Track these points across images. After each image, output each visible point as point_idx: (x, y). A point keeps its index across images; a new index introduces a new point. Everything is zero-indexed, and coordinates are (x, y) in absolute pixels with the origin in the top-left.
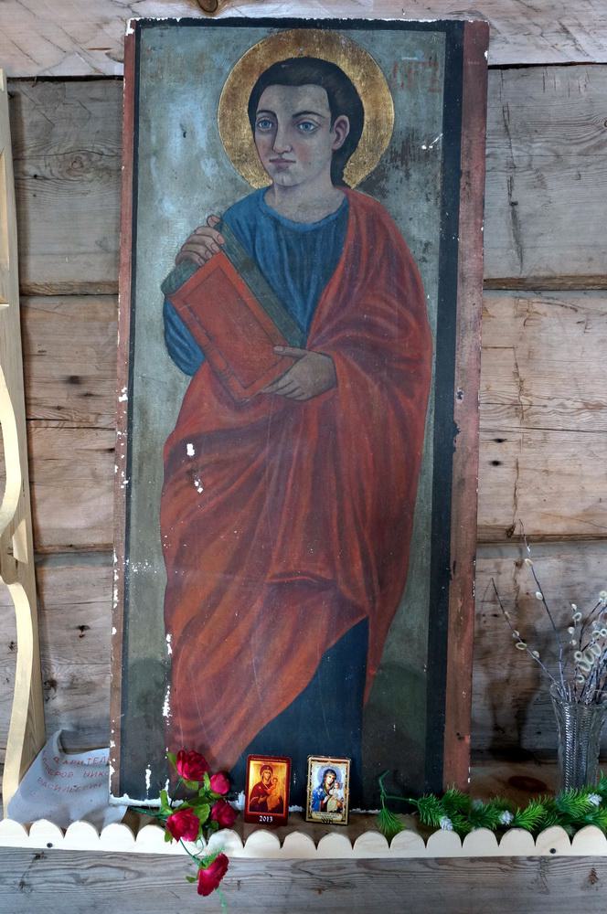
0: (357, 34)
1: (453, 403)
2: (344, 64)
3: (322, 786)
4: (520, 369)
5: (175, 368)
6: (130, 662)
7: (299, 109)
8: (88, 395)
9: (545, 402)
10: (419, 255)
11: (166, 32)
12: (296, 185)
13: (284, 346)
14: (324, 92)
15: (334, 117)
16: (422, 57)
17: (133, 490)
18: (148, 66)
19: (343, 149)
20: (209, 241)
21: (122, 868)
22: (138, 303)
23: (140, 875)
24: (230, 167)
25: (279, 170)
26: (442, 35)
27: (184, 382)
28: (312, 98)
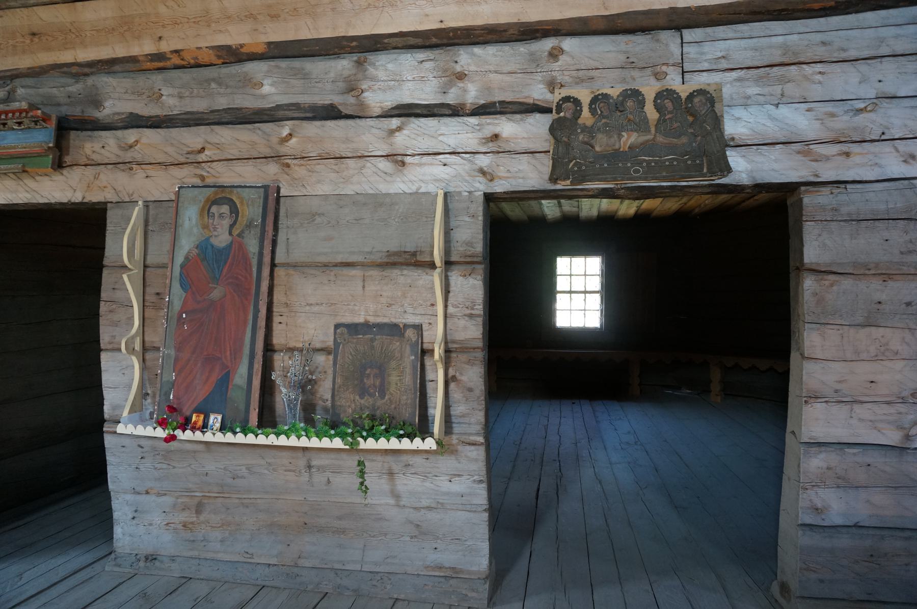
0: (239, 189)
1: (259, 303)
2: (234, 199)
3: (213, 423)
4: (287, 292)
5: (182, 291)
6: (163, 381)
7: (222, 212)
8: (162, 298)
9: (295, 303)
10: (252, 256)
11: (187, 190)
12: (219, 235)
13: (212, 284)
14: (228, 207)
15: (231, 214)
16: (256, 197)
17: (168, 328)
18: (181, 199)
19: (233, 224)
20: (193, 252)
21: (169, 464)
22: (173, 271)
23: (174, 467)
24: (201, 230)
25: (215, 230)
26: (263, 189)
27: (184, 295)
28: (225, 209)
